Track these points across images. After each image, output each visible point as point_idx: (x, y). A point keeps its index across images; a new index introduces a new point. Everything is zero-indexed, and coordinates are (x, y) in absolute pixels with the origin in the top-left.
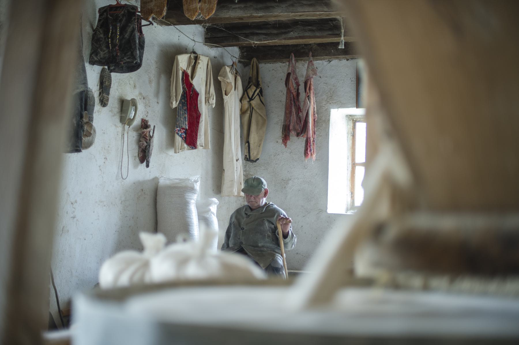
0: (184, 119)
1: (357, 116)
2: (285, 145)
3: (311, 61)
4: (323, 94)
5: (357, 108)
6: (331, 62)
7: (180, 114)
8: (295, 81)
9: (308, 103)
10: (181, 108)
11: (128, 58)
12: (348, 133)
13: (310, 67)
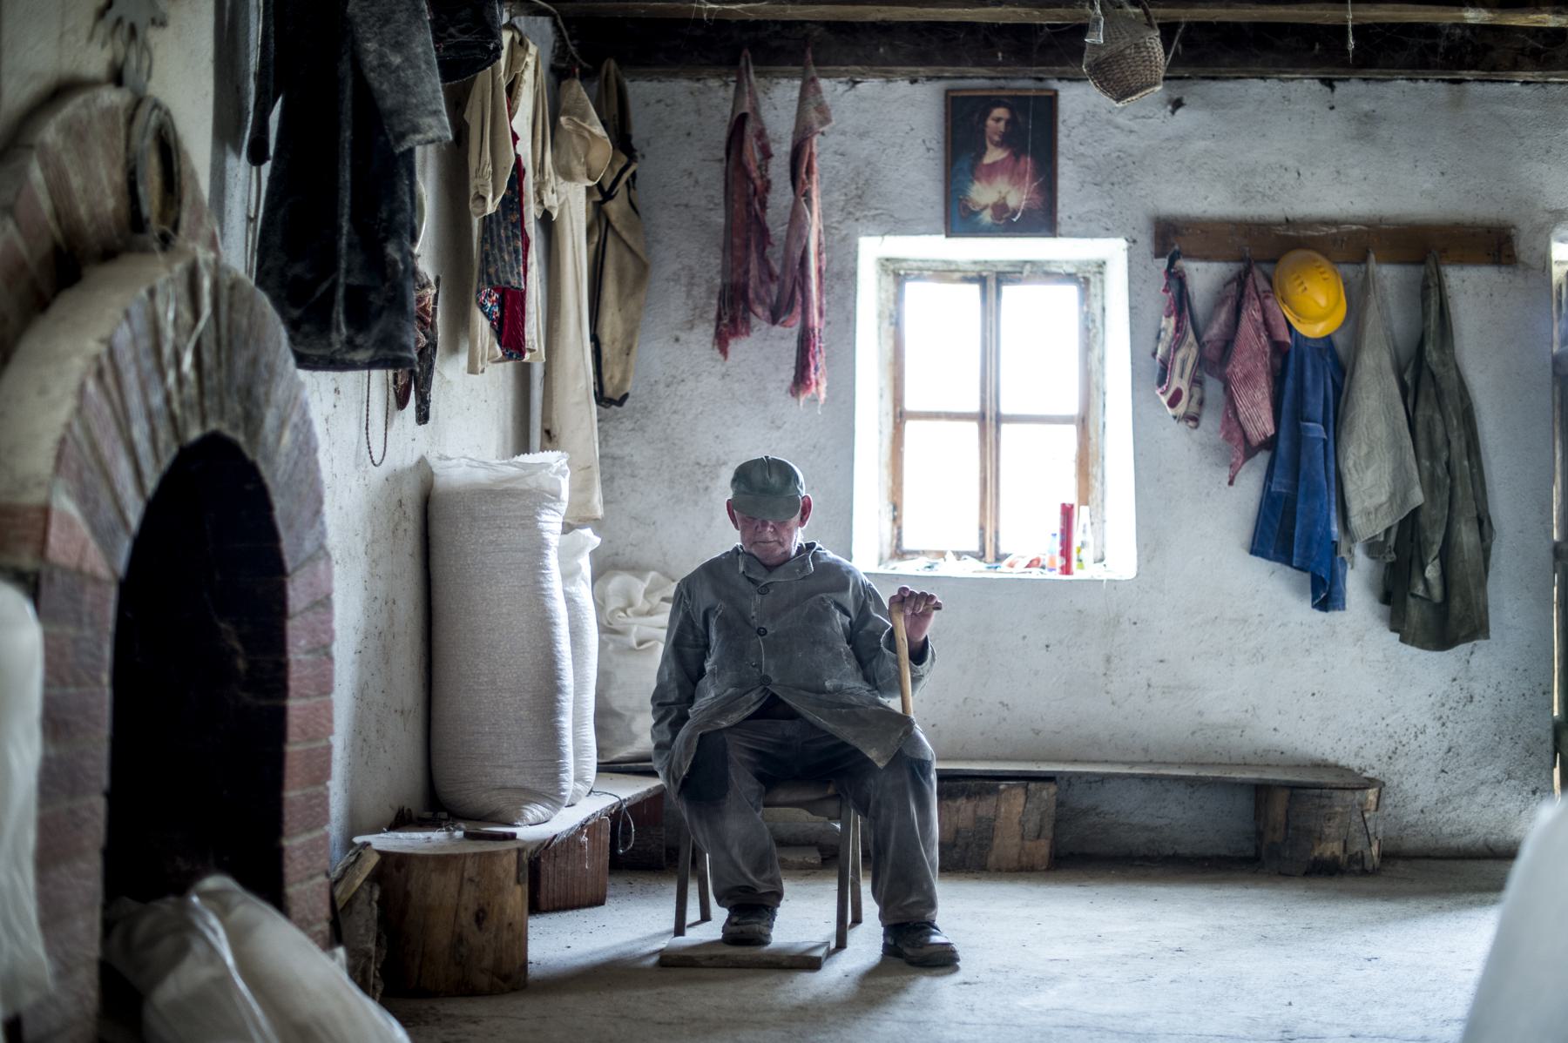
0: (514, 256)
1: (910, 263)
2: (724, 351)
3: (813, 80)
4: (834, 189)
5: (947, 236)
6: (859, 86)
7: (495, 238)
8: (759, 143)
9: (806, 216)
10: (501, 218)
11: (463, 32)
12: (880, 315)
13: (811, 100)
